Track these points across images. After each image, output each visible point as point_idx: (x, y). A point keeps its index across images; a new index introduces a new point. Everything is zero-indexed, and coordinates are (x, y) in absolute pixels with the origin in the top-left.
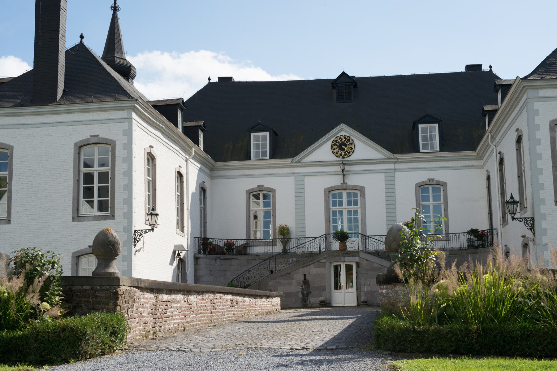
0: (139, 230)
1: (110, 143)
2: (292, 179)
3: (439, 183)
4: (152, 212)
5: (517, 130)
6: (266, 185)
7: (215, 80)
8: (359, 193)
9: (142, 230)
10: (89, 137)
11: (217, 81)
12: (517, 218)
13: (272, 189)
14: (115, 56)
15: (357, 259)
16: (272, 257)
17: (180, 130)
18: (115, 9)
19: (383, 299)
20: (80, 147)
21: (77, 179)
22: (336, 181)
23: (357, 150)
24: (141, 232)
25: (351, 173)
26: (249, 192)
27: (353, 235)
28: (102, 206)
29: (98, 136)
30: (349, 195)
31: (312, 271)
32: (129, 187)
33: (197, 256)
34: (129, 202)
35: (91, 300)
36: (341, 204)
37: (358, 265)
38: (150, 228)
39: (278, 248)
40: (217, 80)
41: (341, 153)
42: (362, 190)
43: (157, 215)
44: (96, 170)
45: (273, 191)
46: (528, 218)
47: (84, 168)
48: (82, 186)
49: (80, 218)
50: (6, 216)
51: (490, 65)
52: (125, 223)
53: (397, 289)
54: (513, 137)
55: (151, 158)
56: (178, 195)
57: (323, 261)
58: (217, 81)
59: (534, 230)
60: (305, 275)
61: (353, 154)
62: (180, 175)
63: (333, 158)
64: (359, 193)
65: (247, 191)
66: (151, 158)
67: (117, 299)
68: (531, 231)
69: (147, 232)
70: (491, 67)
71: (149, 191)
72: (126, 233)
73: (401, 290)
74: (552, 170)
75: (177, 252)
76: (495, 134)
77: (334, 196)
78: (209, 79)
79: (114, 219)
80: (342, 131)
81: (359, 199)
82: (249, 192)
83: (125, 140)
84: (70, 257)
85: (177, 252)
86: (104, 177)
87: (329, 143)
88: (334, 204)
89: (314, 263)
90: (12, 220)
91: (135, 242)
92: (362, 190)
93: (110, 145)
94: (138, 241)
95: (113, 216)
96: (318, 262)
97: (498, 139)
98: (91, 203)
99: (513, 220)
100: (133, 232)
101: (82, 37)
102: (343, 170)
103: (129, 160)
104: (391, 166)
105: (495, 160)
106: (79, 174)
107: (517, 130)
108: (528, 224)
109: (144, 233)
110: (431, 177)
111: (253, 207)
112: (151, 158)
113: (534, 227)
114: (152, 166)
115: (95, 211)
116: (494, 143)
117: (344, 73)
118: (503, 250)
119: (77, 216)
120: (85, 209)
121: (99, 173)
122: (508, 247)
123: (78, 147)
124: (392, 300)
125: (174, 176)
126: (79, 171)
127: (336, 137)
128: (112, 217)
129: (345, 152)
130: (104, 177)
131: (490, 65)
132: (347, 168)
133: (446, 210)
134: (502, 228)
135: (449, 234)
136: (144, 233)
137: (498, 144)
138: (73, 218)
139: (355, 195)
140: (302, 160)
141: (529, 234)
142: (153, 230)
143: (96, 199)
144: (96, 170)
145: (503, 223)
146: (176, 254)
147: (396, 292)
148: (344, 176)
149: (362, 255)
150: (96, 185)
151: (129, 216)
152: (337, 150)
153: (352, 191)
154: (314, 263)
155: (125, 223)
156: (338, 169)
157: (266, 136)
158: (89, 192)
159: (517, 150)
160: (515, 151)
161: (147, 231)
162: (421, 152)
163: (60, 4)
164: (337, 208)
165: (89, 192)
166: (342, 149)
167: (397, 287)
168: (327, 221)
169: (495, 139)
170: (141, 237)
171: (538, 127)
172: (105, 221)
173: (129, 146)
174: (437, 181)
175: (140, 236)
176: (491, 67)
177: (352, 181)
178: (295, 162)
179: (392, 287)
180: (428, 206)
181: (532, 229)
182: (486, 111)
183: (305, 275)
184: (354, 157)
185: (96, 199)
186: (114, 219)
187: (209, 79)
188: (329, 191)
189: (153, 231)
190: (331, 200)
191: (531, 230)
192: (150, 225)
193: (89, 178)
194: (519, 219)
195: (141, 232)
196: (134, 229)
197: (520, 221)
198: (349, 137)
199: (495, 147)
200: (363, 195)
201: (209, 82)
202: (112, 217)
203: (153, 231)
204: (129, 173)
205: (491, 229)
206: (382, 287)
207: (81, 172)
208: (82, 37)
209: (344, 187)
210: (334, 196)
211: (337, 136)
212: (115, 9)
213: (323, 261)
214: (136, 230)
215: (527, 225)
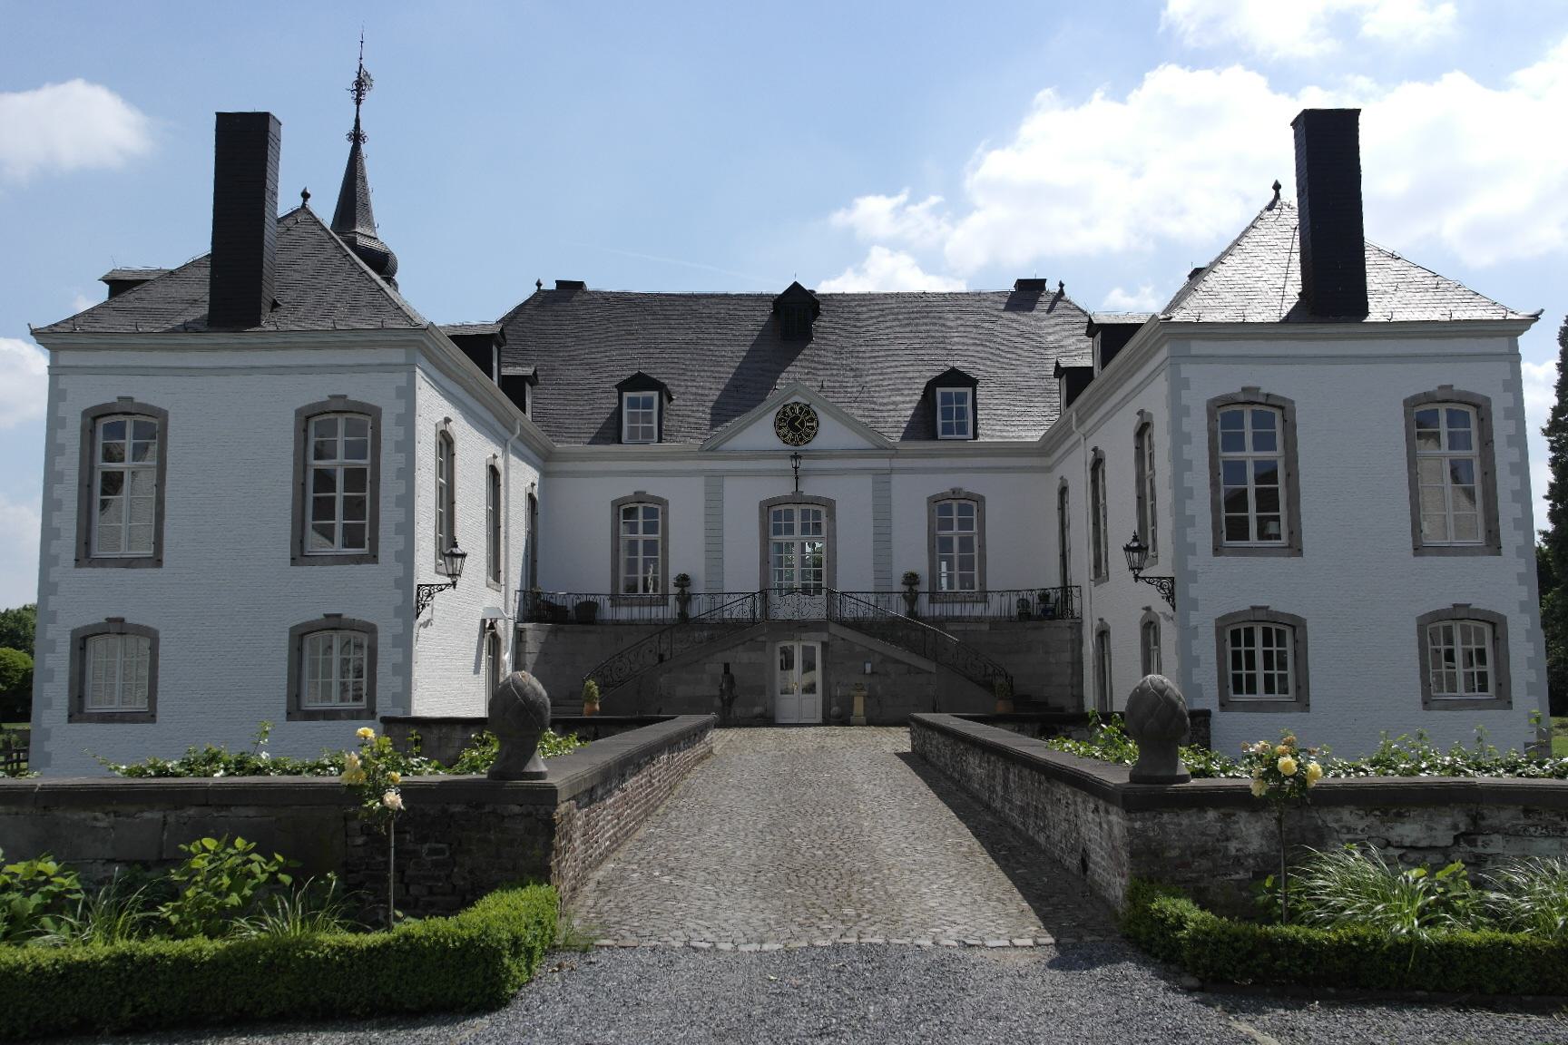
0: (427, 586)
1: (374, 413)
2: (699, 482)
3: (969, 497)
4: (449, 551)
5: (1141, 413)
6: (651, 492)
7: (549, 285)
8: (823, 511)
9: (433, 585)
10: (325, 398)
11: (554, 288)
12: (1144, 578)
13: (661, 499)
14: (356, 230)
15: (825, 637)
16: (661, 627)
17: (496, 384)
18: (357, 137)
19: (1136, 841)
20: (306, 417)
21: (302, 481)
22: (784, 488)
23: (822, 430)
24: (432, 589)
25: (808, 472)
26: (616, 504)
27: (1348, 816)
28: (353, 538)
29: (345, 396)
30: (805, 514)
31: (741, 657)
32: (407, 501)
33: (520, 625)
34: (407, 528)
35: (493, 837)
36: (790, 530)
37: (824, 644)
38: (448, 580)
39: (670, 611)
40: (553, 286)
41: (794, 435)
42: (830, 505)
43: (463, 556)
44: (338, 464)
45: (663, 502)
46: (1164, 578)
47: (315, 459)
48: (311, 495)
49: (306, 558)
50: (152, 552)
51: (1060, 282)
52: (399, 571)
53: (1163, 821)
54: (1133, 423)
55: (446, 440)
56: (441, 483)
57: (761, 639)
58: (554, 288)
59: (1173, 600)
60: (727, 666)
61: (816, 437)
62: (494, 472)
63: (776, 443)
64: (823, 511)
65: (613, 503)
66: (446, 444)
67: (552, 833)
68: (1169, 601)
69: (442, 590)
70: (1061, 285)
71: (441, 507)
72: (401, 591)
73: (1171, 823)
74: (1209, 491)
75: (488, 622)
76: (1084, 414)
77: (777, 516)
78: (539, 284)
79: (377, 563)
80: (795, 394)
81: (824, 520)
82: (616, 504)
83: (400, 407)
84: (287, 636)
85: (488, 622)
86: (356, 478)
87: (771, 417)
88: (777, 531)
89: (745, 642)
90: (165, 558)
91: (418, 607)
92: (830, 505)
93: (370, 415)
94: (424, 606)
95: (375, 556)
96: (752, 640)
97: (1090, 423)
98: (327, 533)
99: (1136, 581)
100: (416, 588)
101: (305, 195)
102: (796, 468)
103: (407, 446)
104: (884, 463)
105: (1083, 460)
106: (305, 472)
107: (1141, 413)
108: (1163, 589)
109: (436, 590)
110: (956, 485)
111: (625, 535)
112: (446, 444)
113: (1173, 594)
114: (447, 458)
115: (337, 548)
116: (1082, 430)
117: (796, 286)
118: (1094, 628)
119: (300, 556)
120: (315, 543)
121: (345, 469)
122: (1106, 624)
123: (303, 418)
124: (1154, 844)
125: (483, 474)
126: (305, 466)
127: (785, 406)
128: (373, 558)
129: (800, 434)
130: (356, 478)
131: (1060, 282)
132: (804, 464)
133: (982, 547)
134: (1093, 587)
135: (987, 592)
136: (436, 590)
137: (1089, 434)
138: (293, 559)
139: (817, 514)
140: (722, 444)
141: (1160, 606)
142: (454, 584)
143: (339, 522)
144: (338, 464)
145: (1096, 577)
146: (487, 626)
147: (1162, 826)
148: (797, 478)
149: (834, 628)
150: (340, 494)
151: (407, 557)
152: (784, 431)
153: (811, 507)
154: (744, 643)
155: (399, 571)
156: (788, 464)
157: (652, 398)
158: (324, 509)
159: (1137, 448)
160: (1134, 450)
161: (443, 587)
162: (939, 438)
163: (268, 127)
164: (783, 538)
165: (324, 509)
166: (795, 429)
167: (1165, 816)
168: (765, 561)
169: (1083, 422)
170: (430, 598)
171: (1186, 411)
172: (357, 567)
173: (408, 419)
174: (1460, 393)
175: (428, 596)
176: (1061, 285)
177: (811, 488)
178: (707, 450)
179: (1155, 817)
180: (950, 540)
181: (1170, 597)
182: (1063, 368)
183: (727, 666)
184: (818, 443)
185: (339, 522)
186: (377, 563)
187: (539, 284)
188: (767, 506)
189: (454, 588)
190: (772, 522)
191: (1168, 598)
192: (449, 575)
193: (324, 480)
194: (1147, 580)
195: (432, 589)
196: (417, 582)
197: (1149, 583)
198: (808, 406)
199: (1083, 439)
200: (832, 515)
201: (539, 289)
202: (373, 558)
203: (454, 588)
204: (408, 473)
205: (1065, 588)
206: (1133, 815)
207: (308, 468)
208: (305, 195)
209: (797, 499)
210: (777, 516)
211: (786, 403)
212: (357, 137)
213: (761, 639)
214: (421, 585)
215: (1162, 591)
